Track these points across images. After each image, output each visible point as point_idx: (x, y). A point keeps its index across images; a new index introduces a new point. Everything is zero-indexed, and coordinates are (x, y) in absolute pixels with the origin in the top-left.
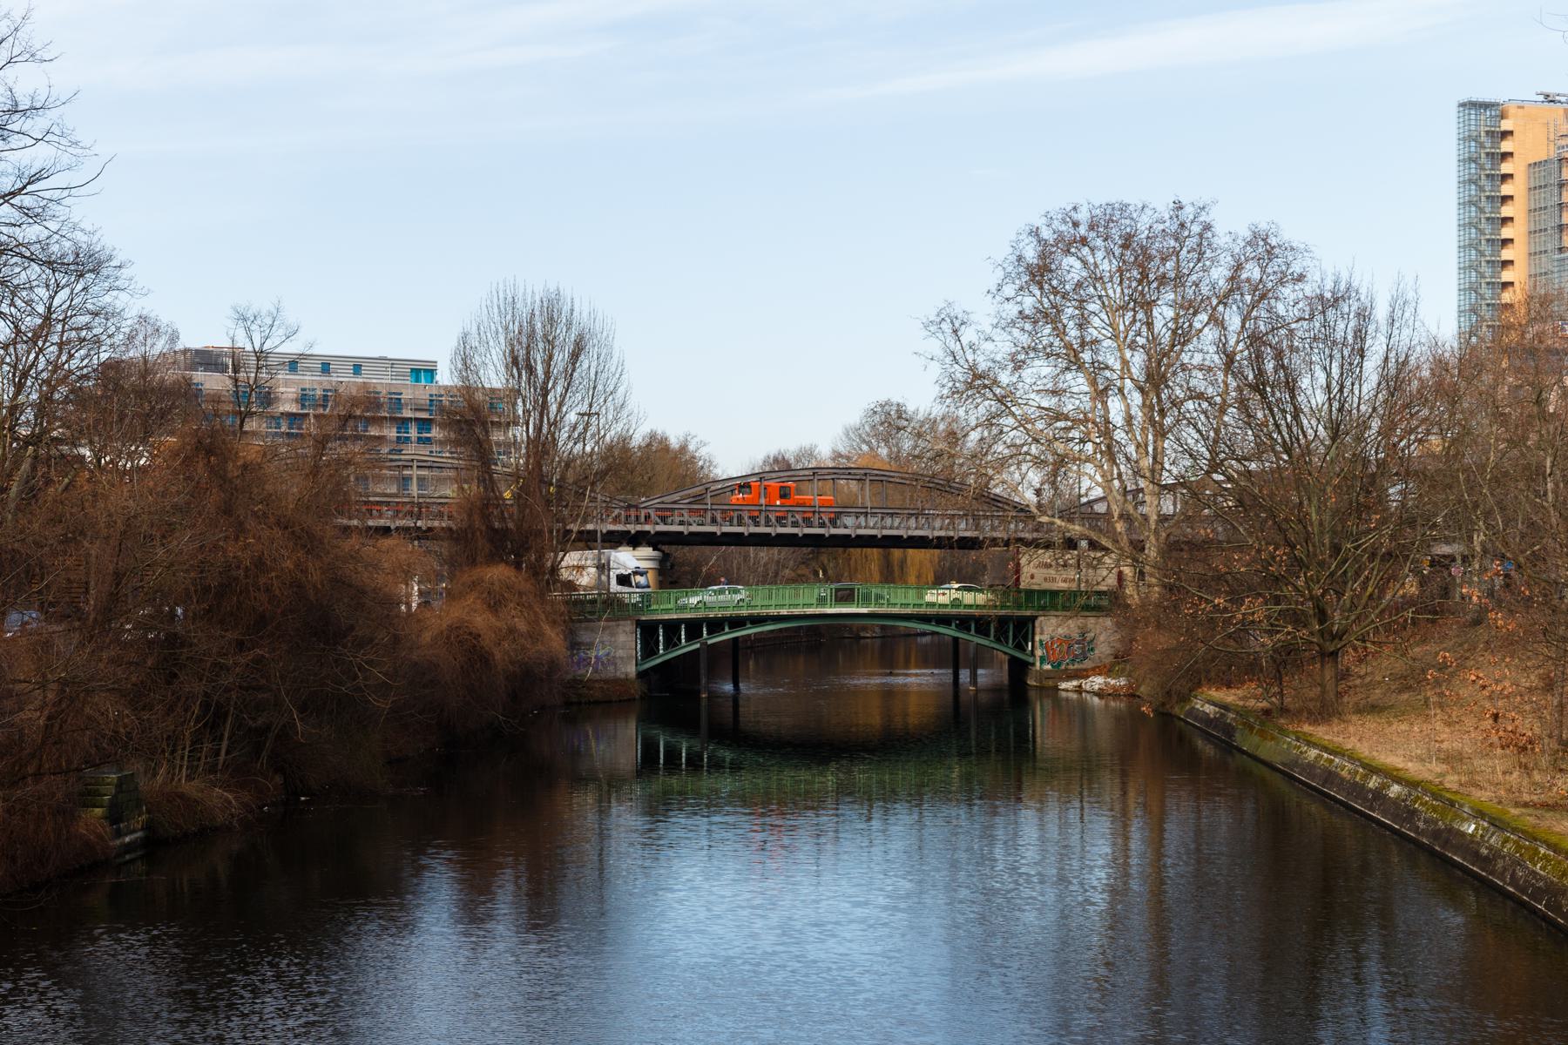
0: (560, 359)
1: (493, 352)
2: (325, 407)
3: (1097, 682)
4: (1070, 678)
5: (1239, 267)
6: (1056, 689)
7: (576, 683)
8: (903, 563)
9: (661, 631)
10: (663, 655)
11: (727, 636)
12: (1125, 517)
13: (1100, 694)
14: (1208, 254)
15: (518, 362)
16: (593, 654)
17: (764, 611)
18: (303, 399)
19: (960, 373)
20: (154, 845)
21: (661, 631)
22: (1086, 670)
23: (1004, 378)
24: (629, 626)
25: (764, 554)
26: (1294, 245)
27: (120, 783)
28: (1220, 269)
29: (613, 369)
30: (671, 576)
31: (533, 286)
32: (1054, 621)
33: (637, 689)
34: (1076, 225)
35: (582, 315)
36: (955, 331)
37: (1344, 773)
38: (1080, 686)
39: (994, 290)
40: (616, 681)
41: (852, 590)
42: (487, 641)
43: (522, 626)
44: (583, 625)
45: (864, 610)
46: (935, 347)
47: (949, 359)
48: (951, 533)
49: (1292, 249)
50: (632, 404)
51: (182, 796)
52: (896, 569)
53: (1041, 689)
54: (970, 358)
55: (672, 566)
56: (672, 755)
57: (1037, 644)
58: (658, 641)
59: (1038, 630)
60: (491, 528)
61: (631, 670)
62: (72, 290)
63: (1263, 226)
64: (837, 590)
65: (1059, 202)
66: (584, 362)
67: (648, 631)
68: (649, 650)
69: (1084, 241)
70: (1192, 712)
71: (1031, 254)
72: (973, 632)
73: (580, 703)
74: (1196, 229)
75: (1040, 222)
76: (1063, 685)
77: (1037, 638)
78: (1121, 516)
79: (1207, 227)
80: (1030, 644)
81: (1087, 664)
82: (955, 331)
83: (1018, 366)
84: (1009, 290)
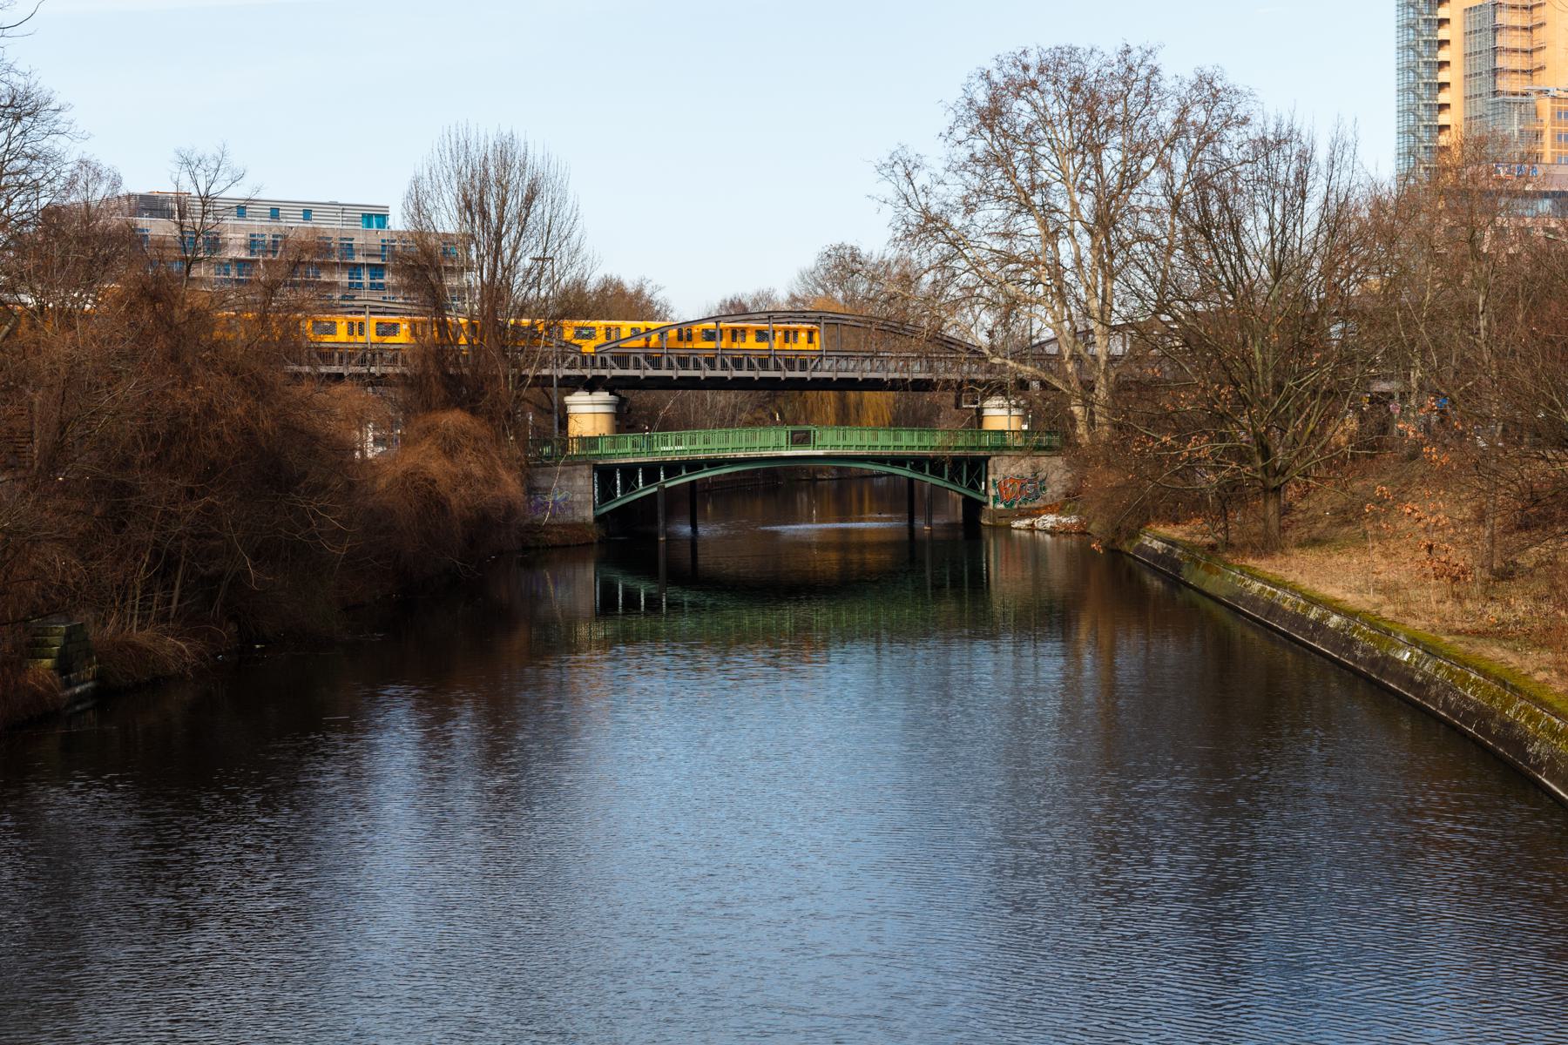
0: (514, 204)
1: (446, 196)
2: (274, 252)
3: (1049, 520)
4: (1022, 516)
5: (1185, 110)
6: (1009, 527)
7: (534, 528)
8: (859, 404)
9: (618, 475)
10: (621, 499)
11: (684, 479)
12: (1077, 358)
13: (1052, 532)
14: (1155, 97)
15: (471, 206)
16: (550, 499)
17: (721, 455)
18: (252, 245)
19: (913, 217)
20: (105, 695)
21: (618, 475)
22: (1038, 509)
23: (957, 221)
24: (586, 471)
25: (723, 398)
26: (1239, 88)
27: (68, 635)
28: (1167, 112)
29: (567, 214)
30: (625, 420)
31: (485, 131)
32: (1006, 460)
33: (594, 534)
34: (1026, 68)
35: (536, 157)
36: (908, 175)
37: (1286, 605)
38: (1032, 525)
39: (945, 133)
40: (574, 526)
41: (808, 432)
42: (443, 486)
43: (477, 471)
44: (540, 470)
45: (820, 452)
46: (888, 190)
47: (902, 202)
48: (905, 376)
49: (1237, 92)
50: (586, 249)
51: (133, 646)
52: (853, 411)
53: (994, 528)
54: (923, 201)
55: (629, 410)
56: (631, 600)
57: (990, 484)
58: (615, 485)
59: (991, 470)
60: (445, 373)
61: (589, 514)
62: (10, 134)
63: (1208, 70)
64: (793, 433)
65: (1009, 45)
66: (538, 207)
67: (605, 475)
68: (606, 494)
69: (1034, 85)
70: (1142, 549)
71: (982, 98)
72: (927, 473)
73: (537, 548)
74: (1143, 72)
75: (991, 66)
76: (1016, 524)
77: (990, 478)
78: (1071, 357)
79: (1154, 71)
80: (983, 483)
81: (1038, 503)
82: (908, 175)
83: (970, 209)
84: (961, 133)
